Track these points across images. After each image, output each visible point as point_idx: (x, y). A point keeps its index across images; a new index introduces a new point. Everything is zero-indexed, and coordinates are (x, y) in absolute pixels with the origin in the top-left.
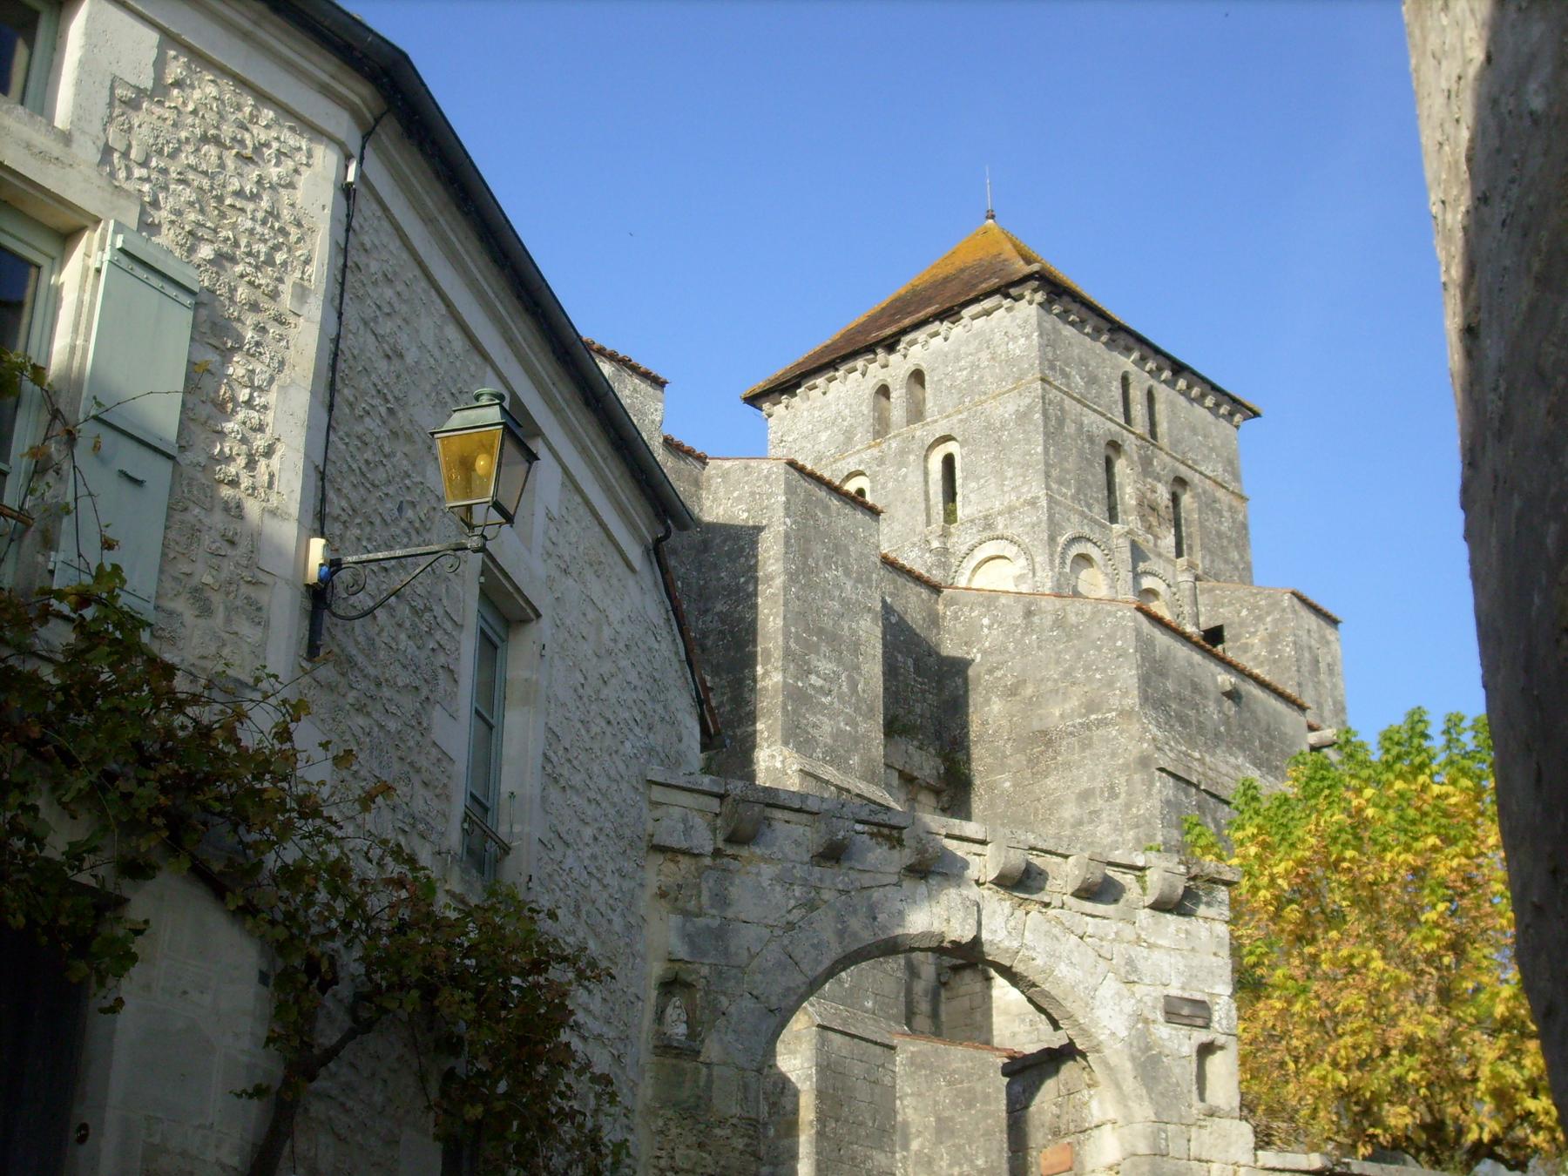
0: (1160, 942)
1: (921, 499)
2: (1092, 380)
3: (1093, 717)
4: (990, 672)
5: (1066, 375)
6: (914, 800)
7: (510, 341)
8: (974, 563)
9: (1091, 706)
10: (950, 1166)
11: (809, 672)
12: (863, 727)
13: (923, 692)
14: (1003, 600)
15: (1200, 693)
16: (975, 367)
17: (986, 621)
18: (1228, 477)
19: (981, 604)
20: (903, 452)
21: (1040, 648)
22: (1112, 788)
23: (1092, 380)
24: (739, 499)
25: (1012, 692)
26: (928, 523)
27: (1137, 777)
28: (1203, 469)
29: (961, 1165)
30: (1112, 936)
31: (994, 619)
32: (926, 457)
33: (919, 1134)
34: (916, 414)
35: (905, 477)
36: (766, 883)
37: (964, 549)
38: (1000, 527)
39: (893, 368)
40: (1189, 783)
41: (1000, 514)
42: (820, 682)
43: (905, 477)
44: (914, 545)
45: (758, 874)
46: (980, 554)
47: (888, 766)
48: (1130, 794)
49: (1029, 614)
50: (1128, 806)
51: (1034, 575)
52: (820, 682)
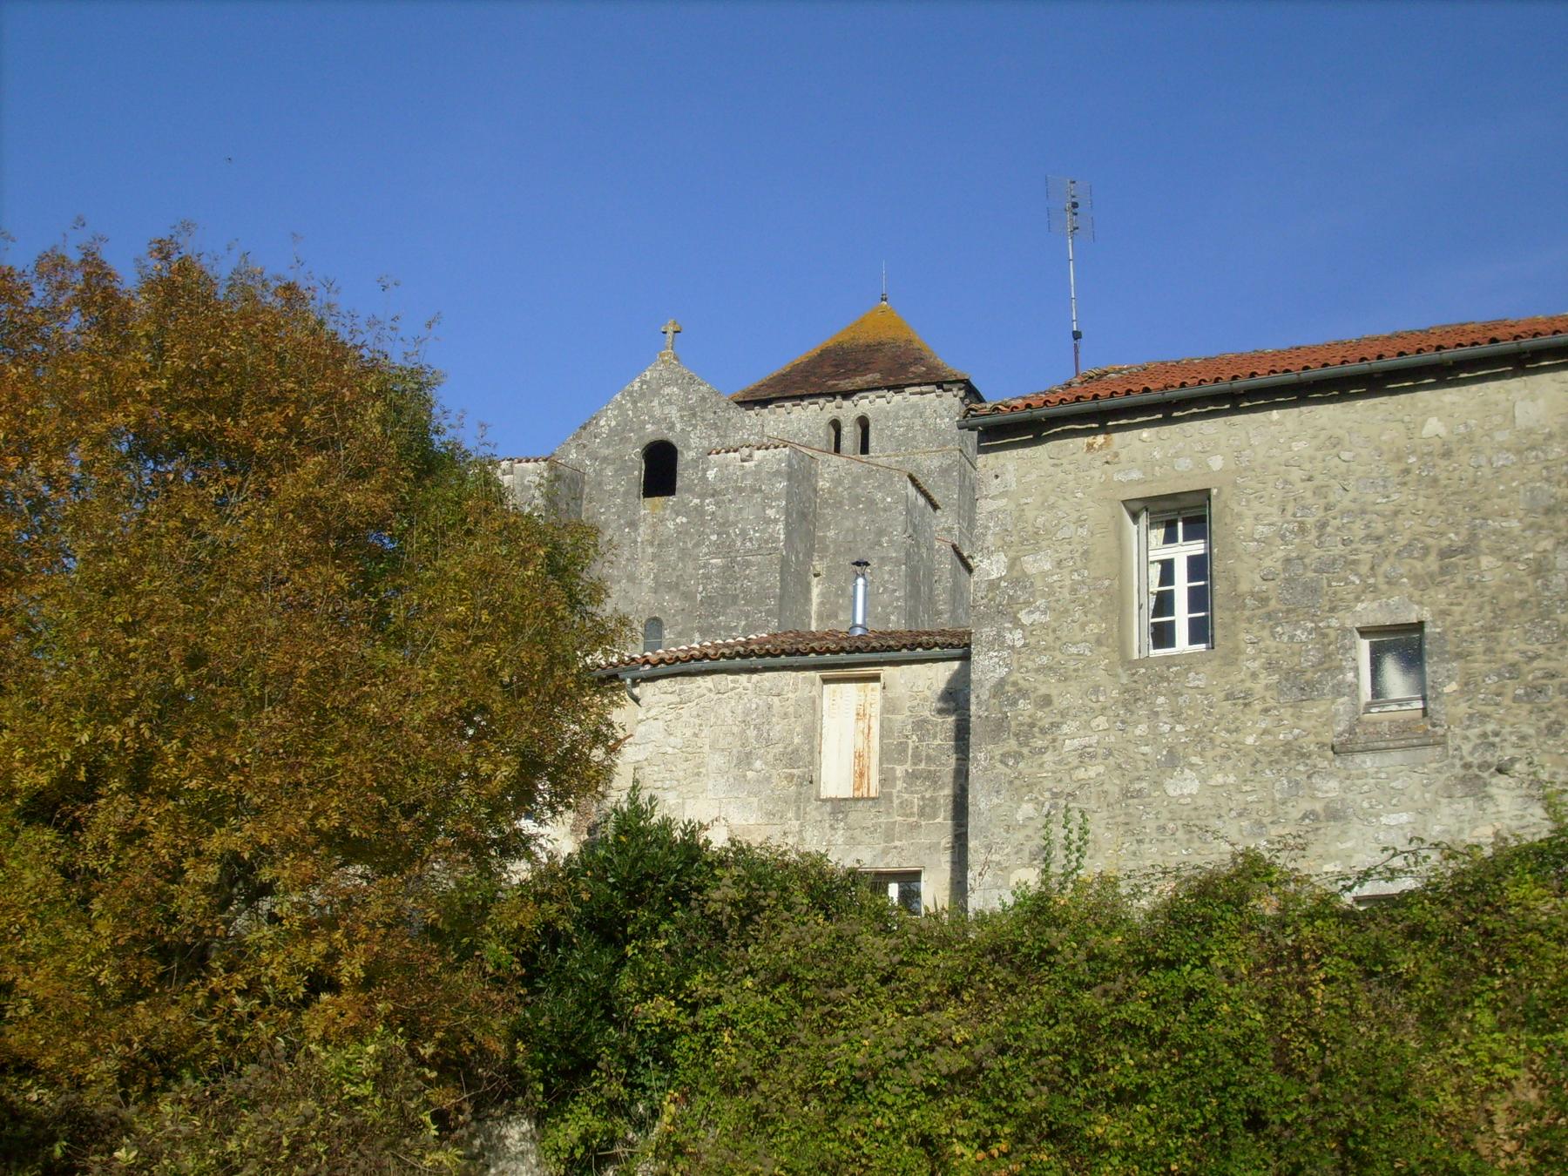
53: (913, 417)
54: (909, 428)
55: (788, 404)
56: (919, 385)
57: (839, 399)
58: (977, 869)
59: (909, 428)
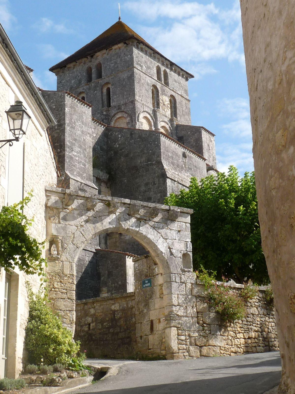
0: (173, 229)
1: (101, 100)
2: (148, 68)
3: (149, 163)
4: (121, 150)
5: (142, 66)
6: (100, 185)
7: (14, 81)
8: (115, 119)
9: (149, 160)
10: (112, 284)
11: (73, 151)
12: (87, 166)
13: (102, 155)
14: (124, 130)
15: (178, 156)
16: (116, 63)
17: (120, 136)
18: (185, 95)
19: (118, 131)
20: (96, 87)
21: (135, 144)
22: (154, 182)
23: (148, 68)
24: (53, 103)
25: (127, 155)
26: (103, 107)
27: (161, 179)
28: (178, 92)
29: (114, 284)
30: (161, 227)
31: (122, 136)
32: (102, 89)
33: (103, 276)
34: (99, 76)
35: (96, 94)
36: (76, 215)
37: (113, 114)
38: (123, 108)
39: (93, 64)
40: (175, 181)
41: (123, 105)
42: (75, 154)
43: (96, 94)
44: (99, 113)
45: (74, 213)
46: (118, 116)
47: (93, 176)
48: (159, 184)
49: (131, 134)
50: (158, 187)
51: (132, 122)
52: (75, 154)
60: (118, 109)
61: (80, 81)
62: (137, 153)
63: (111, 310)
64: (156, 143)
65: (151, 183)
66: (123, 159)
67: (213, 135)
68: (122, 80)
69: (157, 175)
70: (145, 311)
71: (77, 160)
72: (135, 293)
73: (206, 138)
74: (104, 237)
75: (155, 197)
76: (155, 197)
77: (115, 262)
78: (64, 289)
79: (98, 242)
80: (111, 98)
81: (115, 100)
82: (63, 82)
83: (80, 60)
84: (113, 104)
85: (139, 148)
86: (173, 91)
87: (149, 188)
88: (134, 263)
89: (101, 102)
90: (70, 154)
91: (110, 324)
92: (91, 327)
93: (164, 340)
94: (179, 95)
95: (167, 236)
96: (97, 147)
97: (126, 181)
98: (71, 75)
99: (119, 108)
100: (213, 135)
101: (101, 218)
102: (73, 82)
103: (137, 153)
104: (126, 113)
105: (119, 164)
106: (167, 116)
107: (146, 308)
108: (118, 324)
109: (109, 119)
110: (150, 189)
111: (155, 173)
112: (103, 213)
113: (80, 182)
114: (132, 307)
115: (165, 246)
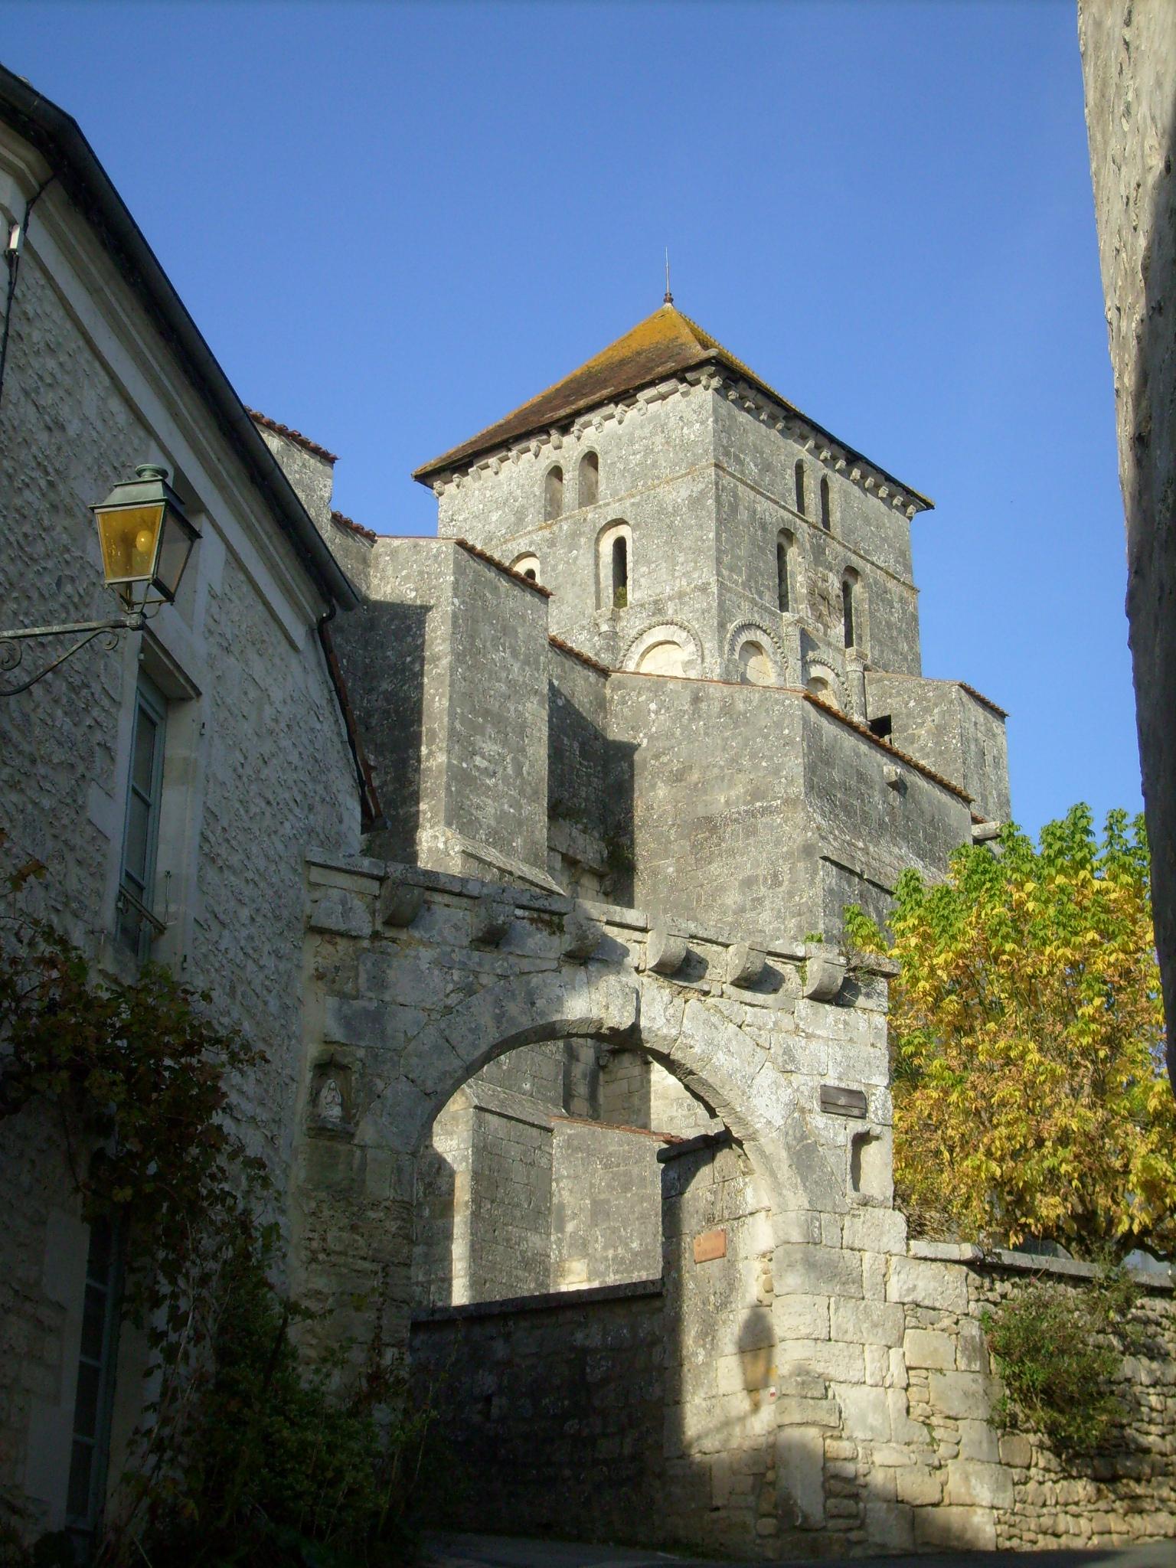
0: (818, 1032)
1: (592, 581)
2: (766, 467)
3: (758, 804)
4: (657, 757)
5: (739, 461)
8: (643, 648)
9: (756, 794)
10: (605, 1248)
12: (527, 810)
14: (671, 686)
17: (653, 706)
20: (575, 535)
21: (706, 734)
22: (775, 876)
24: (407, 578)
25: (678, 777)
26: (598, 607)
28: (875, 559)
29: (616, 1248)
32: (597, 540)
33: (575, 1216)
34: (588, 496)
35: (576, 558)
36: (424, 966)
37: (633, 633)
38: (670, 612)
39: (568, 449)
40: (852, 872)
41: (670, 598)
42: (484, 764)
43: (576, 558)
45: (417, 957)
46: (650, 639)
47: (551, 849)
48: (793, 882)
49: (696, 700)
53: (653, 434)
54: (648, 451)
55: (492, 461)
56: (652, 384)
57: (555, 436)
58: (294, 1170)
59: (648, 451)
60: (654, 614)
61: (520, 517)
62: (716, 771)
63: (573, 1349)
64: (786, 732)
65: (765, 879)
66: (662, 791)
67: (1001, 715)
68: (670, 509)
69: (785, 849)
70: (701, 1358)
71: (488, 788)
72: (664, 1284)
73: (976, 724)
74: (585, 1076)
75: (779, 929)
76: (779, 929)
77: (618, 1165)
78: (365, 1259)
79: (561, 1090)
80: (629, 574)
81: (642, 580)
82: (461, 518)
83: (523, 445)
84: (638, 595)
85: (724, 749)
86: (855, 552)
87: (758, 899)
88: (662, 1166)
89: (593, 589)
90: (464, 765)
91: (566, 1403)
92: (495, 1411)
93: (770, 1475)
94: (878, 567)
95: (792, 1059)
96: (571, 746)
97: (671, 870)
98: (488, 494)
99: (658, 607)
100: (1001, 715)
101: (528, 983)
102: (494, 519)
103: (716, 771)
104: (682, 627)
105: (648, 809)
106: (833, 640)
107: (704, 1346)
108: (597, 1403)
109: (619, 650)
110: (758, 901)
111: (778, 843)
112: (538, 961)
113: (499, 868)
114: (649, 1338)
115: (785, 1099)
